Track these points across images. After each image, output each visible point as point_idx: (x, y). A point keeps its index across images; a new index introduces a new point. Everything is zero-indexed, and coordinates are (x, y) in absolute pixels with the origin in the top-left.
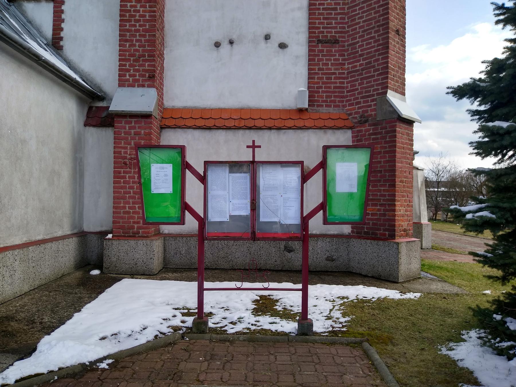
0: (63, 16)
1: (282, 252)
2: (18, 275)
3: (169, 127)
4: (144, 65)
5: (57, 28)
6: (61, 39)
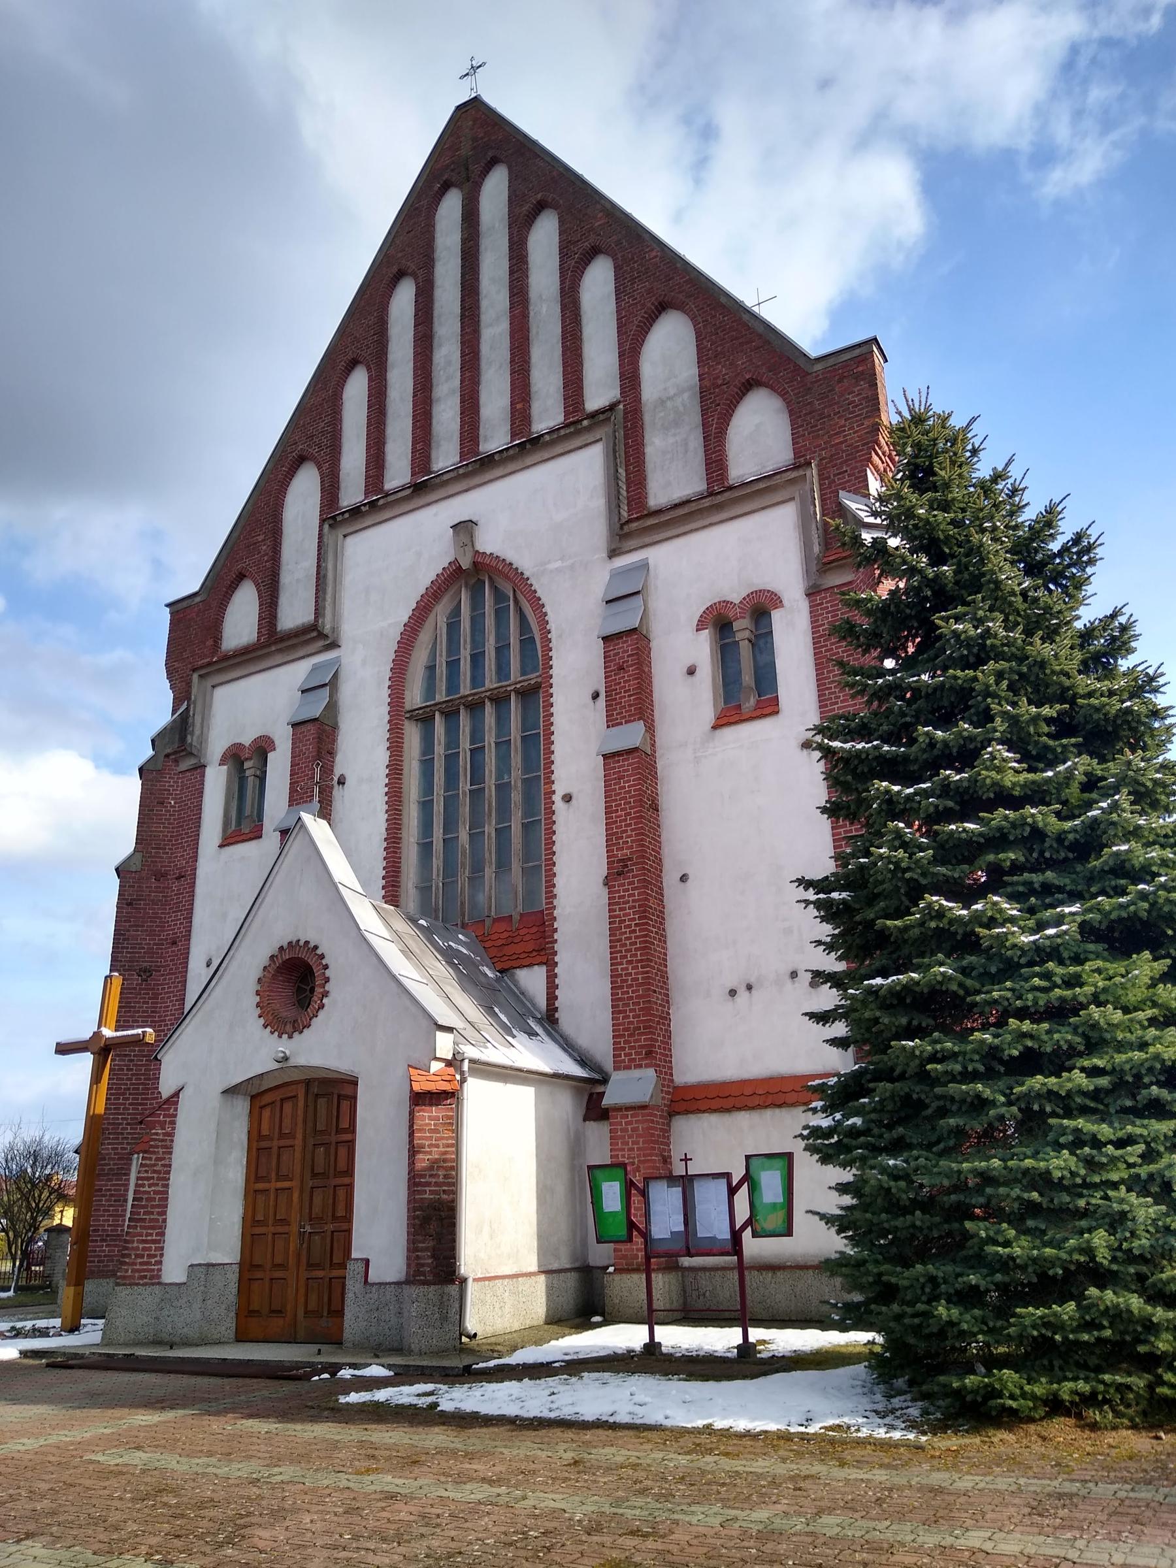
0: (557, 981)
1: (838, 1293)
2: (507, 1309)
3: (679, 1113)
4: (640, 1040)
5: (552, 997)
6: (556, 1009)
